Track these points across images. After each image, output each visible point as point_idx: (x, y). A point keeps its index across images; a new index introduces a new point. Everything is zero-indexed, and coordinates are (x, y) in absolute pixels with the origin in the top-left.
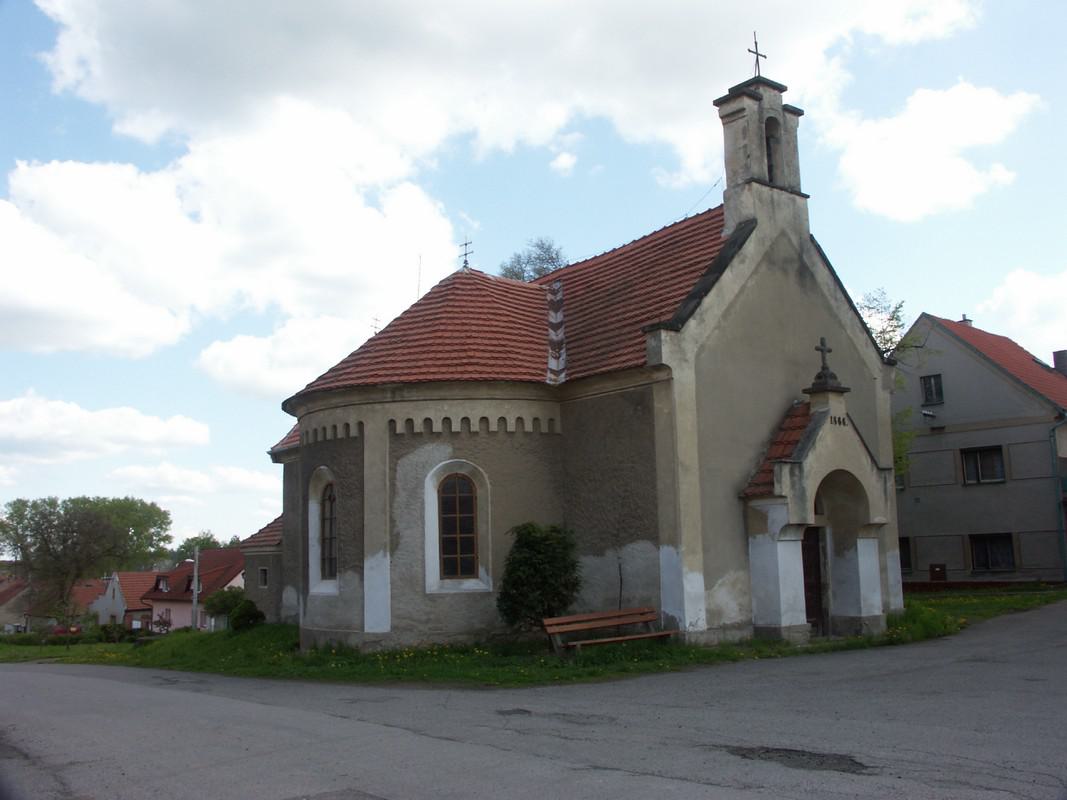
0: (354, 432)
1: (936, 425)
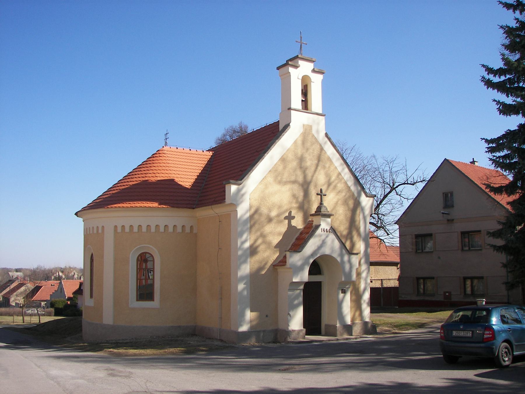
0: (100, 231)
1: (449, 218)
